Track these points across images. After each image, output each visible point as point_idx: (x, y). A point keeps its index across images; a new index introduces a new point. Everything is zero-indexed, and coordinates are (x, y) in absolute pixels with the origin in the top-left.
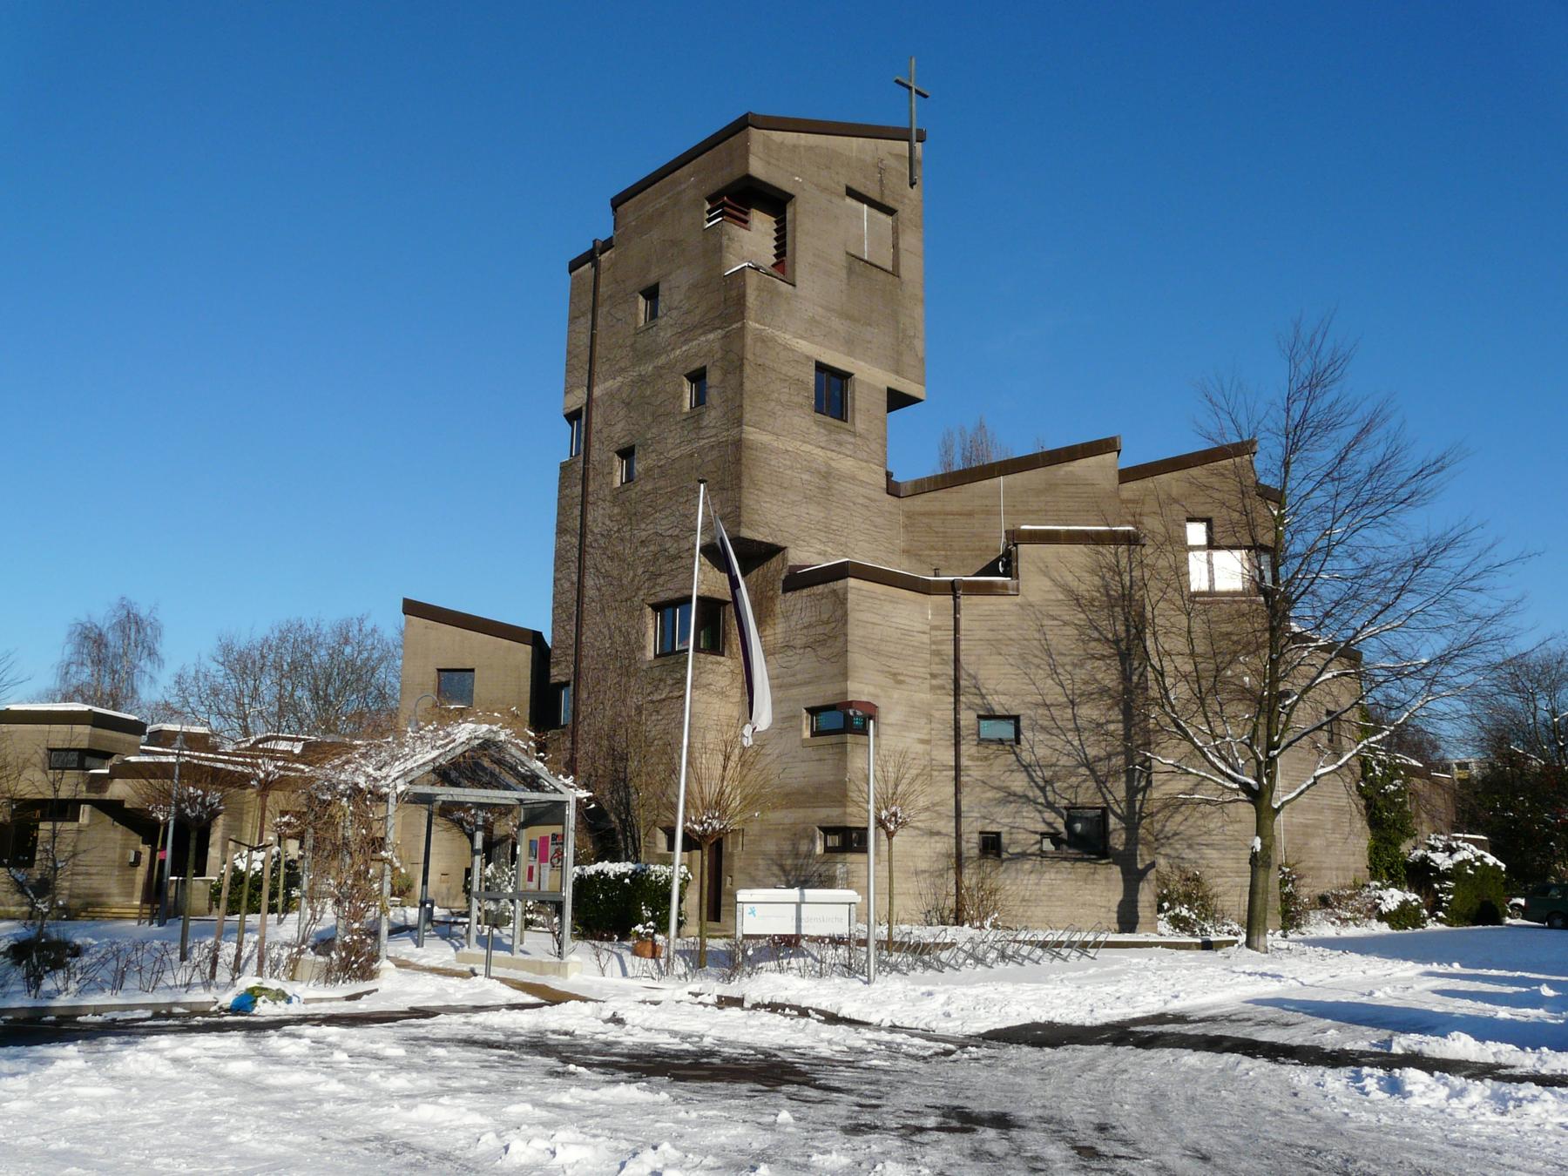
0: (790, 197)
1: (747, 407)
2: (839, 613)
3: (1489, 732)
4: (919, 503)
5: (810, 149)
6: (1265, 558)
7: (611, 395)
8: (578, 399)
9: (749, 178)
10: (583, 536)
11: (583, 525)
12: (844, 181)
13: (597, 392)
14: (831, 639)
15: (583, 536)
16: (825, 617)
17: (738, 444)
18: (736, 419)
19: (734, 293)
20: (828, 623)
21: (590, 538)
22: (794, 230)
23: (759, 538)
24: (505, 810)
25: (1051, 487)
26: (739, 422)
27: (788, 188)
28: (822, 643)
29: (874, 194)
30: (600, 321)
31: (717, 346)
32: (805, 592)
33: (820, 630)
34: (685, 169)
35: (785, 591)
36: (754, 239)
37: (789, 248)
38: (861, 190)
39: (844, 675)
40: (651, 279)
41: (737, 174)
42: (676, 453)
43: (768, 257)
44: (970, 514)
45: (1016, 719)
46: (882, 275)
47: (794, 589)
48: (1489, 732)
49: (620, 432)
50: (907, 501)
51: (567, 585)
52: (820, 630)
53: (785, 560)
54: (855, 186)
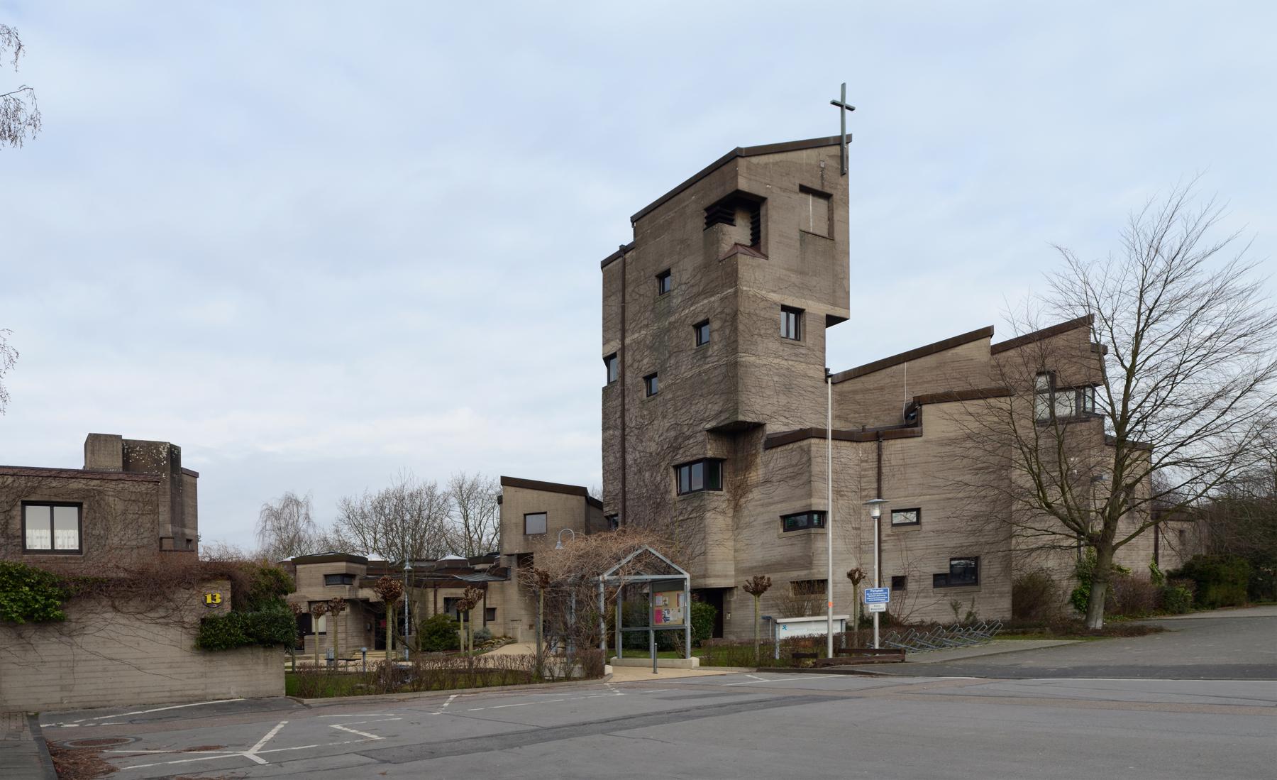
1: (741, 341)
2: (805, 459)
4: (847, 386)
5: (776, 164)
6: (792, 316)
7: (637, 342)
8: (615, 346)
10: (624, 429)
11: (623, 423)
12: (798, 182)
13: (628, 341)
14: (803, 475)
15: (624, 429)
16: (794, 462)
17: (736, 364)
18: (732, 346)
21: (627, 430)
22: (767, 221)
23: (749, 420)
24: (644, 583)
25: (940, 366)
26: (735, 351)
27: (762, 193)
28: (793, 478)
29: (817, 187)
30: (627, 297)
31: (716, 305)
33: (791, 470)
34: (688, 192)
35: (766, 449)
36: (738, 232)
37: (762, 234)
38: (809, 185)
40: (664, 266)
41: (729, 190)
42: (688, 374)
44: (882, 389)
45: (918, 510)
46: (823, 242)
47: (772, 448)
49: (646, 365)
51: (612, 459)
52: (791, 470)
53: (764, 431)
54: (805, 183)
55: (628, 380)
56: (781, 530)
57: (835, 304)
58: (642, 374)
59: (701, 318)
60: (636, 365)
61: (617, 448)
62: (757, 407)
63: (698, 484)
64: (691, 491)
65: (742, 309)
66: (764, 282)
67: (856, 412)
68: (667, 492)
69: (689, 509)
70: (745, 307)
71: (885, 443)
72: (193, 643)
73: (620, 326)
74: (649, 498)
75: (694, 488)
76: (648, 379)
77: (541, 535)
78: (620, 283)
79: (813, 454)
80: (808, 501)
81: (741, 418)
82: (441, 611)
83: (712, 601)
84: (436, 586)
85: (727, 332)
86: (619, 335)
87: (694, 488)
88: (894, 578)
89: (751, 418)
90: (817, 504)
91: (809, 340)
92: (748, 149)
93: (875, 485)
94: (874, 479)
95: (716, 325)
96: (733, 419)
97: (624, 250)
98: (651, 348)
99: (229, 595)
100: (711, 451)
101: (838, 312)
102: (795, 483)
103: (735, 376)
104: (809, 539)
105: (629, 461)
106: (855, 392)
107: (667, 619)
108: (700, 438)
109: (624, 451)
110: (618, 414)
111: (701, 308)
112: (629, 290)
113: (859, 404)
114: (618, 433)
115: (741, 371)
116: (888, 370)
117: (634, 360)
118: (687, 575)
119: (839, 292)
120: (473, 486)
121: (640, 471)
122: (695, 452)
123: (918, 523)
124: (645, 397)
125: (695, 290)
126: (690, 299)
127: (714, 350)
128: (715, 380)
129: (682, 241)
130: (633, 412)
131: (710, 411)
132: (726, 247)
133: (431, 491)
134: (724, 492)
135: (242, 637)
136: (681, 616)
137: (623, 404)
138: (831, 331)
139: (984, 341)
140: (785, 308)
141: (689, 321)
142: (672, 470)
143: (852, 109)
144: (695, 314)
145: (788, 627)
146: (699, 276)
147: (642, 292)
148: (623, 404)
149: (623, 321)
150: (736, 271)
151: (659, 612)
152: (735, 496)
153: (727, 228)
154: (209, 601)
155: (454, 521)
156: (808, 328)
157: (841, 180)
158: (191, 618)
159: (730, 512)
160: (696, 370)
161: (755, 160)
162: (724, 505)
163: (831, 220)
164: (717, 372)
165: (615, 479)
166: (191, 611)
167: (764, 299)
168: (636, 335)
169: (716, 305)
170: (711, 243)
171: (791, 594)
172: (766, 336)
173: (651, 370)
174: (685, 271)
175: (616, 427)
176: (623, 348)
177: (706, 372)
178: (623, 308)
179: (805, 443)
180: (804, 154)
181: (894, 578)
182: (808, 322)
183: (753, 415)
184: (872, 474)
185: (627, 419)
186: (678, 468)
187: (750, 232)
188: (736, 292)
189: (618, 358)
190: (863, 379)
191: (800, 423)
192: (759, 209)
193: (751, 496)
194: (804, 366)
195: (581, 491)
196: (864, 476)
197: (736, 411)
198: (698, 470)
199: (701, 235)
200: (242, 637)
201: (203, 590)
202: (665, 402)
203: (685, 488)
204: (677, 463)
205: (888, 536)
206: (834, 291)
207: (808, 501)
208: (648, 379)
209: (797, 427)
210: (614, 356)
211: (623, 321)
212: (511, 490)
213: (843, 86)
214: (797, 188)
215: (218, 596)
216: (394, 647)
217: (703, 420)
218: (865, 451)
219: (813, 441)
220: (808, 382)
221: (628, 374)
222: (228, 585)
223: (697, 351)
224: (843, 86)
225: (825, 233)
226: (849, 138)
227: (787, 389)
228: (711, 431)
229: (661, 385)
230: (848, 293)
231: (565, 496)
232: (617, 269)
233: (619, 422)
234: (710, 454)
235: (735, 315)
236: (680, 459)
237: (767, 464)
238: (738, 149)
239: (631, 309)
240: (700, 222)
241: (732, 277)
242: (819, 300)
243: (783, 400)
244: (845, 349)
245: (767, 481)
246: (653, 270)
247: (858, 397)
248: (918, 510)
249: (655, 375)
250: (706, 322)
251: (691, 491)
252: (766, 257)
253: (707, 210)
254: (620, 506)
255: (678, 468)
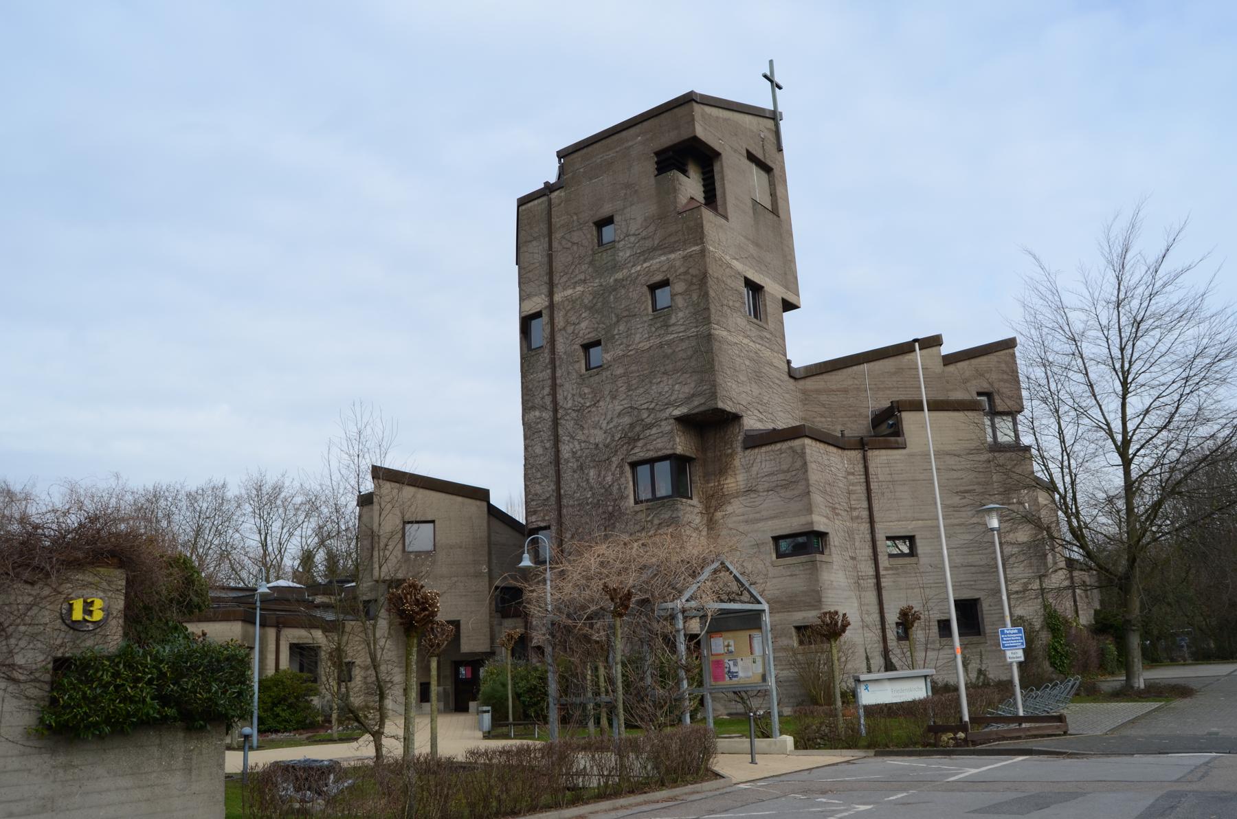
0: (718, 155)
2: (798, 464)
3: (139, 547)
4: (810, 384)
5: (725, 120)
8: (538, 303)
9: (695, 139)
10: (555, 411)
11: (555, 402)
12: (745, 146)
13: (557, 298)
14: (795, 481)
15: (555, 411)
16: (785, 467)
17: (709, 337)
19: (692, 224)
20: (788, 471)
21: (561, 412)
22: (723, 179)
23: (728, 409)
25: (899, 371)
26: (707, 321)
28: (785, 487)
30: (555, 244)
31: (678, 263)
32: (764, 449)
33: (781, 476)
34: (632, 131)
36: (690, 186)
37: (719, 193)
39: (809, 510)
40: (605, 211)
41: (685, 135)
43: (700, 196)
44: (846, 391)
45: (911, 539)
48: (139, 547)
49: (586, 328)
50: (802, 382)
51: (539, 450)
52: (781, 476)
53: (741, 425)
55: (560, 348)
58: (580, 341)
59: (658, 278)
60: (570, 329)
61: (546, 434)
62: (734, 394)
63: (664, 489)
64: (655, 498)
66: (728, 243)
67: (822, 416)
68: (623, 497)
69: (656, 522)
70: (713, 270)
71: (870, 453)
72: (28, 719)
73: (546, 279)
74: (597, 505)
75: (659, 494)
76: (586, 347)
77: (428, 553)
78: (543, 226)
79: (808, 458)
80: (808, 518)
81: (720, 405)
82: (284, 663)
84: (279, 625)
85: (695, 297)
86: (545, 289)
87: (659, 494)
88: (939, 622)
89: (729, 407)
90: (820, 523)
91: (771, 325)
92: (702, 96)
93: (865, 505)
94: (863, 496)
95: (679, 287)
96: (710, 405)
97: (548, 188)
98: (591, 309)
99: (120, 604)
100: (681, 445)
101: (791, 298)
102: (789, 494)
103: (710, 351)
104: (814, 568)
105: (565, 451)
106: (818, 391)
107: (733, 675)
108: (667, 427)
109: (557, 440)
110: (547, 391)
111: (658, 264)
112: (557, 235)
113: (824, 406)
114: (547, 415)
115: (716, 345)
116: (850, 370)
117: (567, 323)
118: (765, 606)
119: (789, 277)
120: (277, 489)
121: (581, 468)
122: (661, 445)
123: (913, 553)
124: (583, 371)
125: (648, 243)
126: (642, 253)
127: (679, 317)
128: (681, 355)
129: (628, 186)
130: (568, 393)
131: (680, 394)
132: (683, 200)
133: (218, 492)
134: (695, 501)
135: (152, 708)
136: (759, 669)
137: (554, 378)
138: (788, 316)
139: (934, 349)
141: (642, 280)
142: (627, 468)
143: (780, 88)
144: (649, 272)
145: (871, 687)
146: (652, 228)
147: (575, 240)
148: (554, 378)
149: (551, 273)
151: (718, 664)
152: (707, 508)
154: (78, 615)
155: (246, 536)
156: (769, 310)
158: (31, 657)
160: (655, 341)
163: (773, 195)
164: (684, 345)
165: (545, 477)
166: (33, 637)
167: (730, 266)
168: (570, 292)
169: (678, 263)
170: (666, 193)
171: (796, 644)
173: (592, 336)
174: (634, 218)
175: (543, 408)
176: (551, 306)
177: (669, 343)
178: (550, 257)
179: (797, 443)
180: (747, 119)
181: (939, 622)
182: (768, 303)
184: (861, 489)
185: (560, 397)
186: (634, 465)
187: (702, 189)
189: (545, 318)
190: (825, 376)
191: (773, 421)
192: (711, 165)
193: (730, 509)
195: (481, 495)
196: (854, 492)
197: (714, 395)
198: (663, 469)
199: (652, 180)
200: (152, 708)
201: (66, 588)
202: (615, 379)
203: (645, 494)
204: (635, 459)
205: (886, 569)
207: (808, 518)
208: (586, 347)
209: (770, 426)
210: (538, 315)
211: (551, 273)
212: (387, 486)
213: (771, 62)
215: (98, 603)
216: (564, 720)
217: (669, 404)
218: (849, 460)
220: (775, 373)
221: (560, 340)
222: (119, 578)
223: (655, 318)
224: (771, 62)
228: (680, 420)
229: (608, 357)
231: (460, 499)
232: (536, 212)
233: (548, 400)
234: (679, 450)
235: (703, 278)
236: (639, 453)
237: (746, 469)
238: (692, 93)
239: (561, 260)
240: (651, 167)
241: (698, 234)
244: (809, 339)
245: (750, 491)
247: (823, 398)
248: (911, 539)
249: (597, 343)
250: (665, 283)
251: (655, 498)
252: (726, 218)
253: (657, 154)
254: (553, 515)
255: (634, 465)
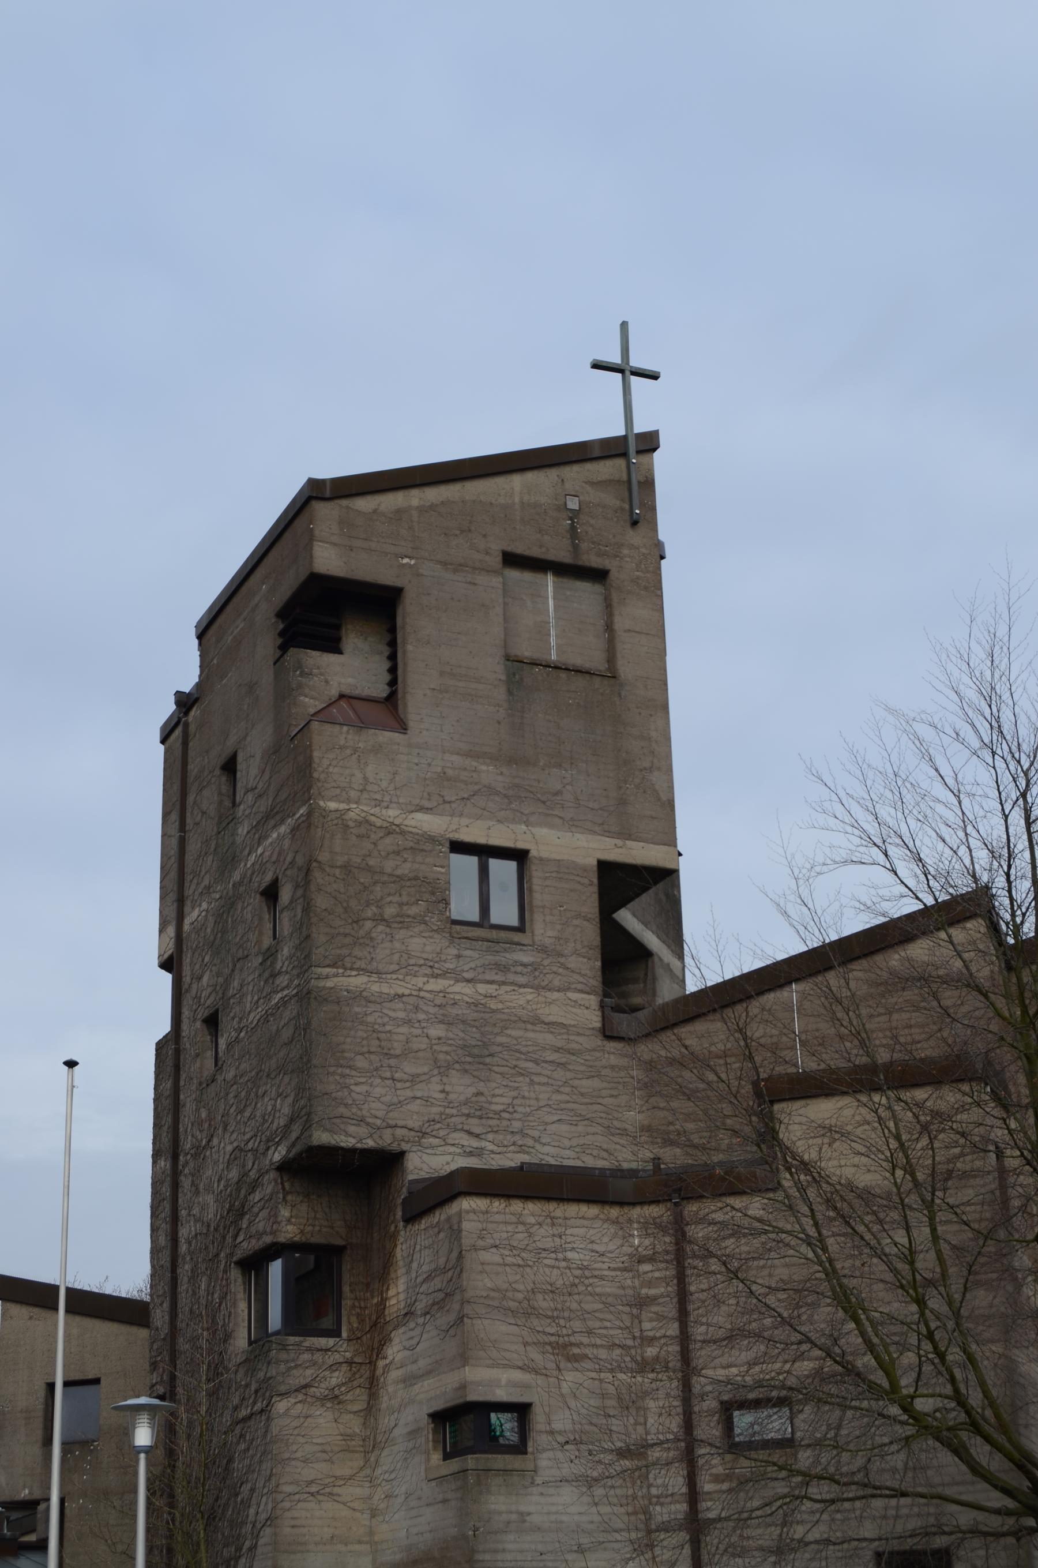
12: (497, 547)
29: (561, 553)
31: (287, 843)
36: (350, 667)
56: (436, 1457)
57: (626, 834)
65: (324, 857)
81: (322, 1137)
83: (800, 1541)
93: (673, 1329)
94: (670, 1309)
108: (269, 1185)
140: (459, 847)
142: (235, 1274)
150: (309, 762)
153: (315, 659)
157: (636, 537)
159: (357, 1400)
161: (364, 504)
162: (335, 1379)
170: (284, 694)
172: (403, 921)
180: (517, 481)
183: (363, 1131)
188: (309, 814)
194: (529, 994)
206: (622, 802)
213: (624, 325)
214: (496, 561)
219: (466, 1203)
224: (624, 325)
225: (593, 658)
226: (649, 443)
227: (476, 1057)
228: (284, 1168)
230: (669, 806)
236: (247, 1246)
242: (573, 825)
243: (461, 1087)
246: (217, 757)
